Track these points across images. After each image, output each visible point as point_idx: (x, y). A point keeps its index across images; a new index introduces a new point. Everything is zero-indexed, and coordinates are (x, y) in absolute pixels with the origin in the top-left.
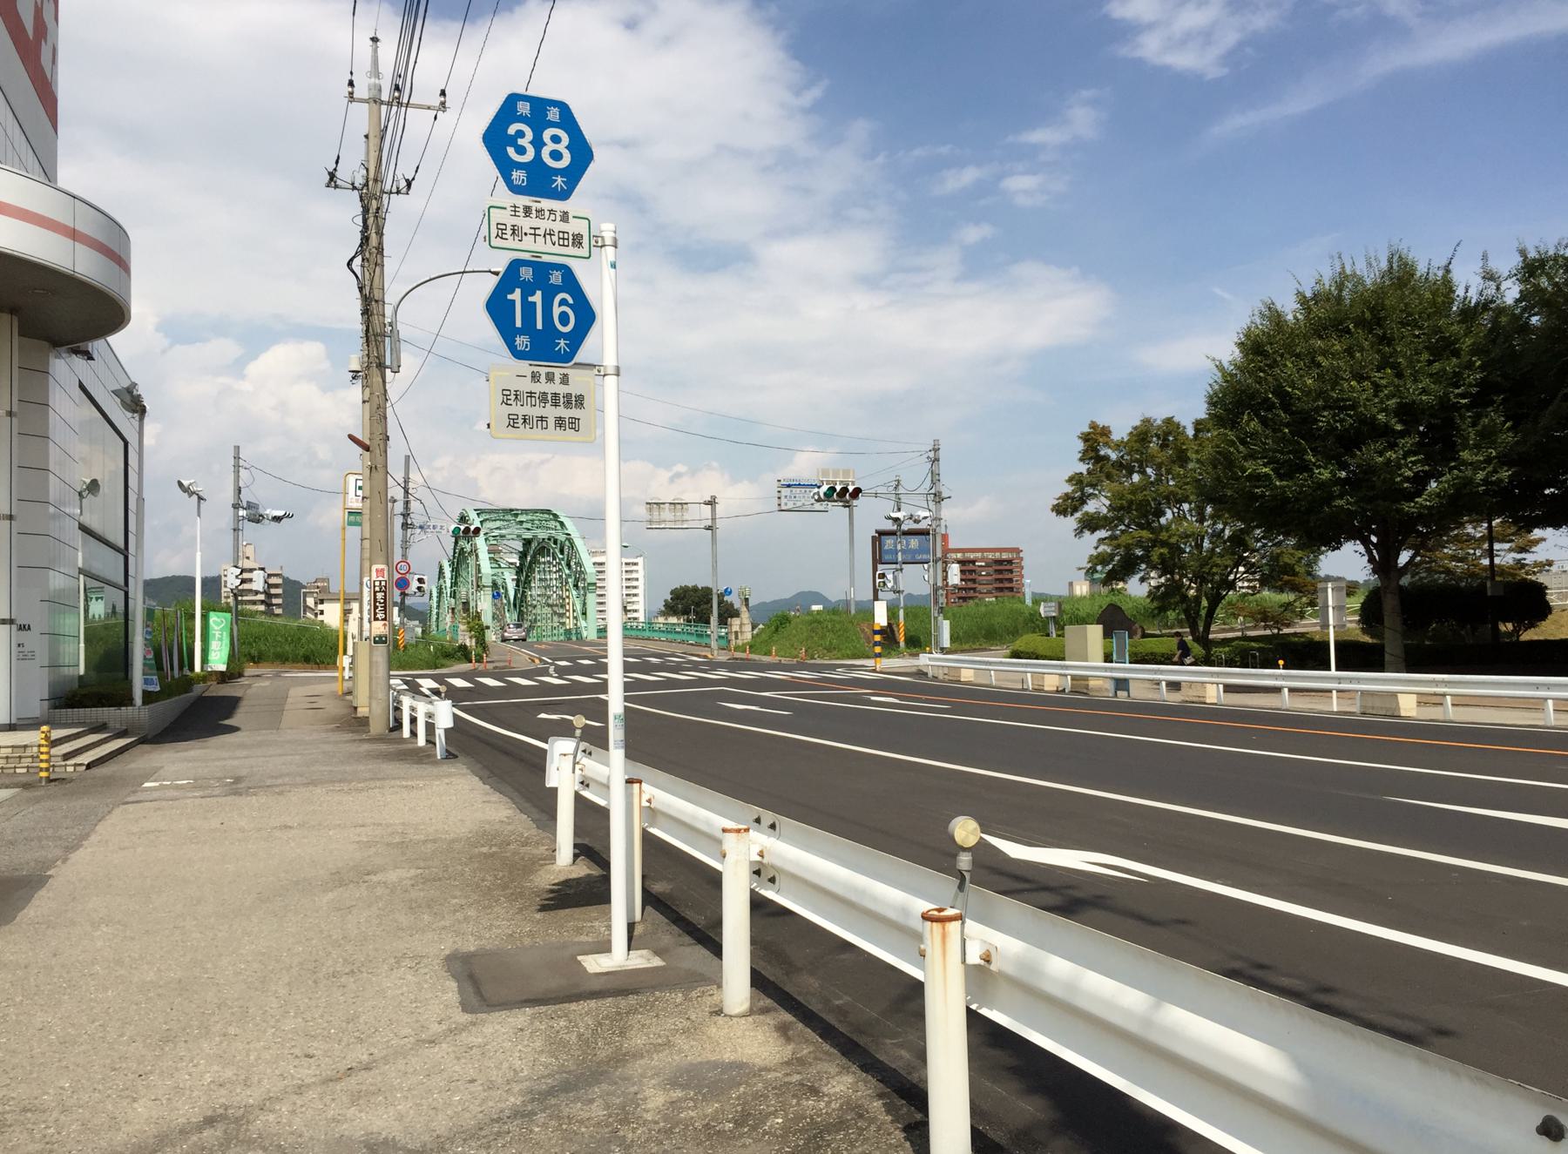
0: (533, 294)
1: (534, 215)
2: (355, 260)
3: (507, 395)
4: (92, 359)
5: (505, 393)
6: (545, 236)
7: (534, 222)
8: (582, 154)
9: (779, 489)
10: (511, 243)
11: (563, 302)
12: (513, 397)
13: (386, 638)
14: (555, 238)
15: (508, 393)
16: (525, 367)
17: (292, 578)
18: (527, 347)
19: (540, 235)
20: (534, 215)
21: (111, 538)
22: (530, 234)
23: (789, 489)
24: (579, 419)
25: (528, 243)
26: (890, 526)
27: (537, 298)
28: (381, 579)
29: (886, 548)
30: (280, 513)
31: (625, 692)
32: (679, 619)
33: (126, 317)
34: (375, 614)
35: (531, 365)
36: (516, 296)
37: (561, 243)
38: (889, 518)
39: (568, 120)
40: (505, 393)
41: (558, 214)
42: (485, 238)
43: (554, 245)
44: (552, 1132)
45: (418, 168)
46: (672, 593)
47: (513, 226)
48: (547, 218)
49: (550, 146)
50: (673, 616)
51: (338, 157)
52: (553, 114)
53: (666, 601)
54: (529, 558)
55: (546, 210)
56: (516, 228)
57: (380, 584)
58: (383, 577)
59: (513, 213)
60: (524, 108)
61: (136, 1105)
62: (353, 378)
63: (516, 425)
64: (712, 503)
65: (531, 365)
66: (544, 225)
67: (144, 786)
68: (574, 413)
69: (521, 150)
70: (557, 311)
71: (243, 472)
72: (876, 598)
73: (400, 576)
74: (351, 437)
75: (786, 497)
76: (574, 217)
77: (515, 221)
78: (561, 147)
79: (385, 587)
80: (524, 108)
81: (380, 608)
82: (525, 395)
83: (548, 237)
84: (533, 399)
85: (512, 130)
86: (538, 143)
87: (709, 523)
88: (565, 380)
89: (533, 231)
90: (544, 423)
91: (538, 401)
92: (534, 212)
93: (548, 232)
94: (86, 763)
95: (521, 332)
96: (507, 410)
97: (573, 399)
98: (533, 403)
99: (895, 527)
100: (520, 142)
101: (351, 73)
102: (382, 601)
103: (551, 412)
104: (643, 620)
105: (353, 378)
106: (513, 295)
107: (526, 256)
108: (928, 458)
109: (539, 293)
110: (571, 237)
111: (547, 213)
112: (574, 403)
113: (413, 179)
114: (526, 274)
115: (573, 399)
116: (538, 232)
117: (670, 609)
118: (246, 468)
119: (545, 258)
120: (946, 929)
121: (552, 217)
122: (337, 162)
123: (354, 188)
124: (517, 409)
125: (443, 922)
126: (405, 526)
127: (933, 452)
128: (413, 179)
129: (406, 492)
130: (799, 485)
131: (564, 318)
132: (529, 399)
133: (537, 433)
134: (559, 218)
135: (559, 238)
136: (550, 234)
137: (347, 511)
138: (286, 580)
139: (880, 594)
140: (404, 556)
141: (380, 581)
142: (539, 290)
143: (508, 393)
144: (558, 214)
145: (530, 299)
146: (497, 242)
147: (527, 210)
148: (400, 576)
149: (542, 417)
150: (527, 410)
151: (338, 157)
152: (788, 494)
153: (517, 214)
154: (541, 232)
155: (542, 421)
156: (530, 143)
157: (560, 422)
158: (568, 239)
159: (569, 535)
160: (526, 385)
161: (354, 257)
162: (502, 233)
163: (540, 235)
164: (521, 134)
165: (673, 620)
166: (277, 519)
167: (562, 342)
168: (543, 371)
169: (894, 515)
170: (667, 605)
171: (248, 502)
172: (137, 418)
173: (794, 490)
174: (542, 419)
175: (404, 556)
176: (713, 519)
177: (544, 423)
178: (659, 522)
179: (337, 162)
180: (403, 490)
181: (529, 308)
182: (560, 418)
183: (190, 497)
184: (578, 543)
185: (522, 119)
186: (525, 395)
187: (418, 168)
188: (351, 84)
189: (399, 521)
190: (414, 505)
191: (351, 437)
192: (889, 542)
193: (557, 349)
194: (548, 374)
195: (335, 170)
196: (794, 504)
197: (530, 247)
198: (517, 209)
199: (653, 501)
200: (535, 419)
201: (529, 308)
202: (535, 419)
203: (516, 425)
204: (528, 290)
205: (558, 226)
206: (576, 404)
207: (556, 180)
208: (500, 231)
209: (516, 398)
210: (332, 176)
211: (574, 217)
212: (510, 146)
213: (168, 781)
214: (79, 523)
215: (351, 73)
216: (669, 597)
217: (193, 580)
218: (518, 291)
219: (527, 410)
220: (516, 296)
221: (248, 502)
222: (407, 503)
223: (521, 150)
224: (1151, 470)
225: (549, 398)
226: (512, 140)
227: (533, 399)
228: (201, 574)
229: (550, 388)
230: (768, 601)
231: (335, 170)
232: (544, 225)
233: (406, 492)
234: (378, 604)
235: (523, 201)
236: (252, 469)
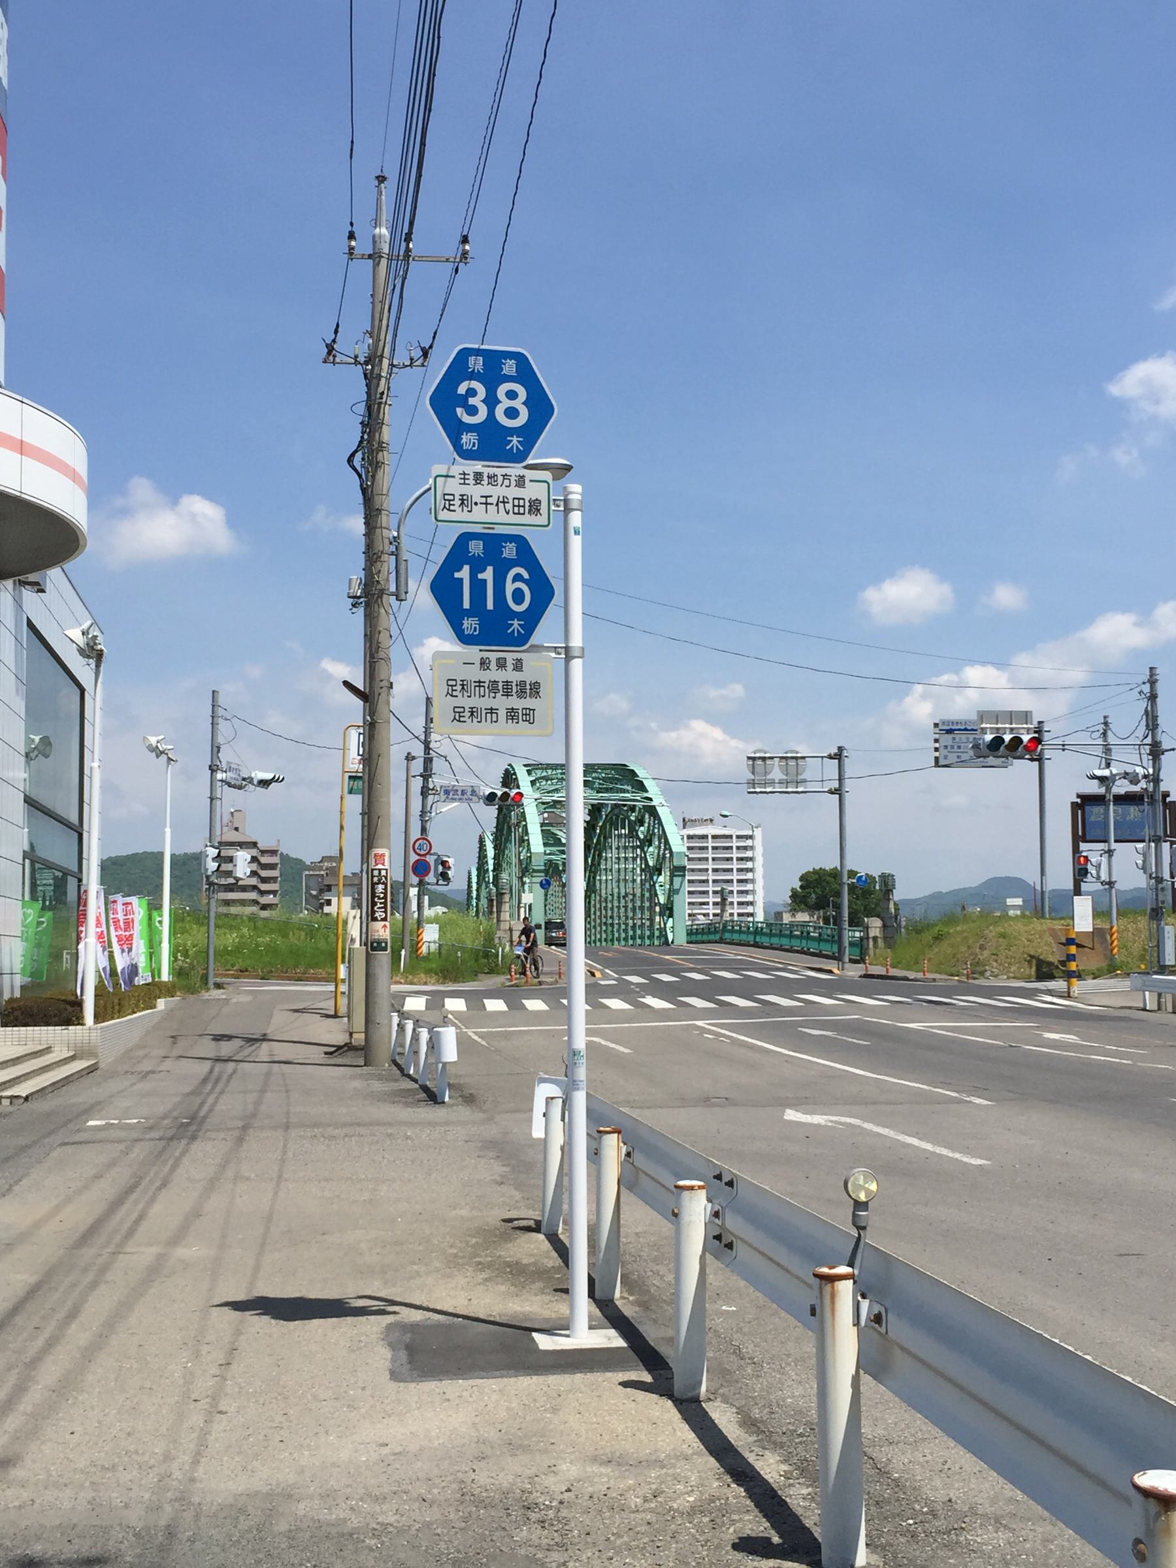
0: (484, 570)
1: (485, 482)
2: (357, 455)
3: (452, 686)
4: (43, 591)
5: (450, 683)
6: (497, 505)
7: (486, 489)
8: (540, 408)
9: (937, 736)
10: (459, 514)
11: (518, 577)
12: (459, 688)
13: (386, 943)
14: (509, 506)
15: (454, 683)
16: (474, 652)
17: (293, 855)
18: (475, 630)
19: (492, 504)
20: (485, 482)
21: (61, 811)
22: (481, 503)
23: (950, 736)
24: (534, 710)
25: (479, 513)
26: (1094, 788)
27: (488, 575)
28: (380, 866)
29: (1093, 819)
30: (269, 776)
31: (586, 1024)
32: (812, 915)
33: (81, 543)
34: (373, 912)
35: (481, 650)
36: (464, 573)
37: (522, 502)
38: (1094, 777)
39: (526, 375)
40: (450, 683)
41: (513, 479)
42: (431, 509)
43: (508, 513)
44: (450, 1494)
45: (435, 333)
46: (801, 879)
47: (462, 495)
48: (500, 484)
49: (505, 403)
50: (802, 911)
51: (338, 325)
52: (509, 367)
53: (793, 890)
54: (598, 831)
55: (499, 476)
56: (465, 497)
57: (380, 873)
58: (383, 864)
59: (462, 481)
60: (476, 364)
61: (43, 1447)
62: (354, 606)
63: (462, 719)
64: (839, 756)
65: (481, 650)
66: (497, 492)
67: (88, 1124)
68: (529, 703)
69: (473, 411)
70: (510, 587)
71: (223, 726)
72: (1077, 891)
73: (418, 857)
74: (347, 684)
75: (946, 747)
76: (531, 481)
77: (465, 490)
78: (518, 404)
79: (386, 878)
80: (476, 364)
81: (379, 905)
82: (473, 684)
83: (501, 505)
84: (482, 689)
85: (462, 389)
86: (491, 401)
87: (836, 785)
88: (519, 665)
89: (484, 500)
90: (494, 715)
91: (487, 690)
92: (485, 478)
93: (501, 499)
94: (24, 1095)
95: (469, 613)
96: (452, 702)
97: (528, 687)
98: (482, 694)
99: (1102, 790)
100: (471, 401)
101: (352, 224)
102: (382, 895)
103: (502, 703)
104: (762, 920)
105: (354, 606)
106: (462, 572)
107: (478, 529)
108: (1141, 692)
109: (490, 569)
110: (527, 504)
111: (500, 479)
112: (528, 691)
113: (431, 347)
114: (476, 548)
115: (528, 687)
116: (489, 500)
117: (799, 900)
118: (226, 719)
119: (499, 530)
120: (836, 1288)
121: (507, 482)
122: (336, 332)
123: (356, 363)
124: (467, 702)
125: (394, 1289)
126: (425, 792)
127: (1148, 685)
128: (431, 347)
129: (427, 748)
130: (966, 729)
131: (518, 596)
132: (477, 688)
133: (486, 726)
134: (513, 483)
135: (514, 506)
136: (504, 502)
137: (347, 775)
138: (285, 858)
139: (1084, 887)
140: (424, 830)
141: (380, 870)
142: (490, 565)
143: (454, 683)
144: (513, 479)
145: (480, 576)
146: (445, 515)
147: (478, 477)
148: (418, 857)
149: (491, 709)
150: (475, 702)
151: (338, 325)
152: (950, 743)
153: (467, 482)
154: (493, 500)
155: (491, 713)
156: (483, 401)
157: (512, 714)
158: (524, 506)
159: (651, 799)
160: (474, 674)
161: (356, 451)
162: (450, 505)
163: (492, 504)
164: (472, 392)
165: (803, 917)
166: (265, 783)
167: (516, 623)
168: (493, 657)
169: (1099, 773)
170: (794, 895)
171: (228, 763)
172: (93, 666)
173: (957, 737)
174: (492, 711)
175: (424, 830)
176: (841, 779)
177: (494, 715)
178: (765, 785)
179: (336, 332)
180: (423, 746)
181: (478, 587)
182: (513, 709)
183: (158, 757)
184: (663, 812)
185: (472, 376)
186: (473, 684)
187: (435, 333)
188: (351, 236)
189: (417, 784)
190: (437, 764)
191: (347, 684)
192: (1095, 812)
193: (509, 631)
194: (498, 660)
195: (334, 341)
196: (958, 757)
197: (480, 517)
198: (467, 477)
199: (758, 755)
200: (484, 712)
201: (478, 587)
202: (484, 712)
203: (462, 719)
204: (477, 567)
205: (513, 492)
206: (530, 693)
207: (511, 441)
208: (447, 502)
209: (463, 688)
210: (330, 349)
211: (531, 481)
212: (458, 407)
213: (115, 1119)
214: (25, 795)
215: (352, 224)
216: (797, 885)
217: (161, 855)
218: (466, 568)
219: (475, 702)
220: (464, 573)
221: (228, 763)
222: (428, 761)
223: (473, 411)
224: (436, 936)
225: (500, 688)
226: (463, 401)
227: (482, 689)
228: (171, 851)
229: (500, 676)
230: (944, 891)
231: (334, 341)
232: (497, 492)
233: (427, 748)
234: (376, 900)
235: (478, 466)
236: (235, 720)
